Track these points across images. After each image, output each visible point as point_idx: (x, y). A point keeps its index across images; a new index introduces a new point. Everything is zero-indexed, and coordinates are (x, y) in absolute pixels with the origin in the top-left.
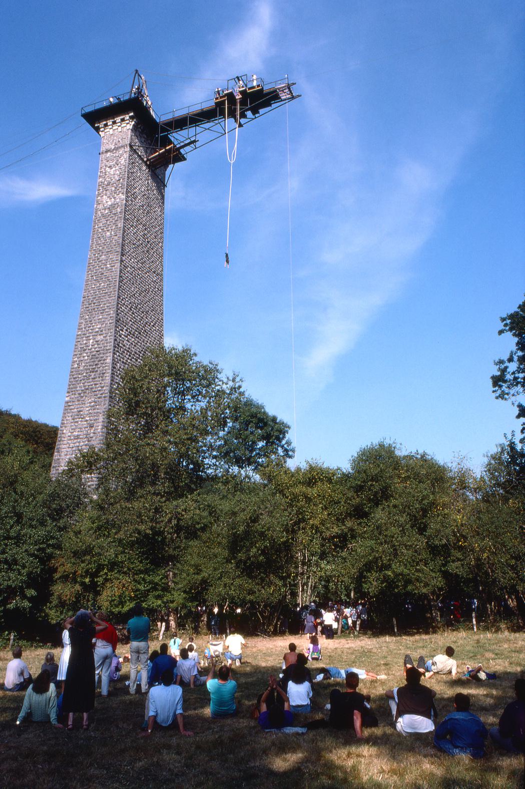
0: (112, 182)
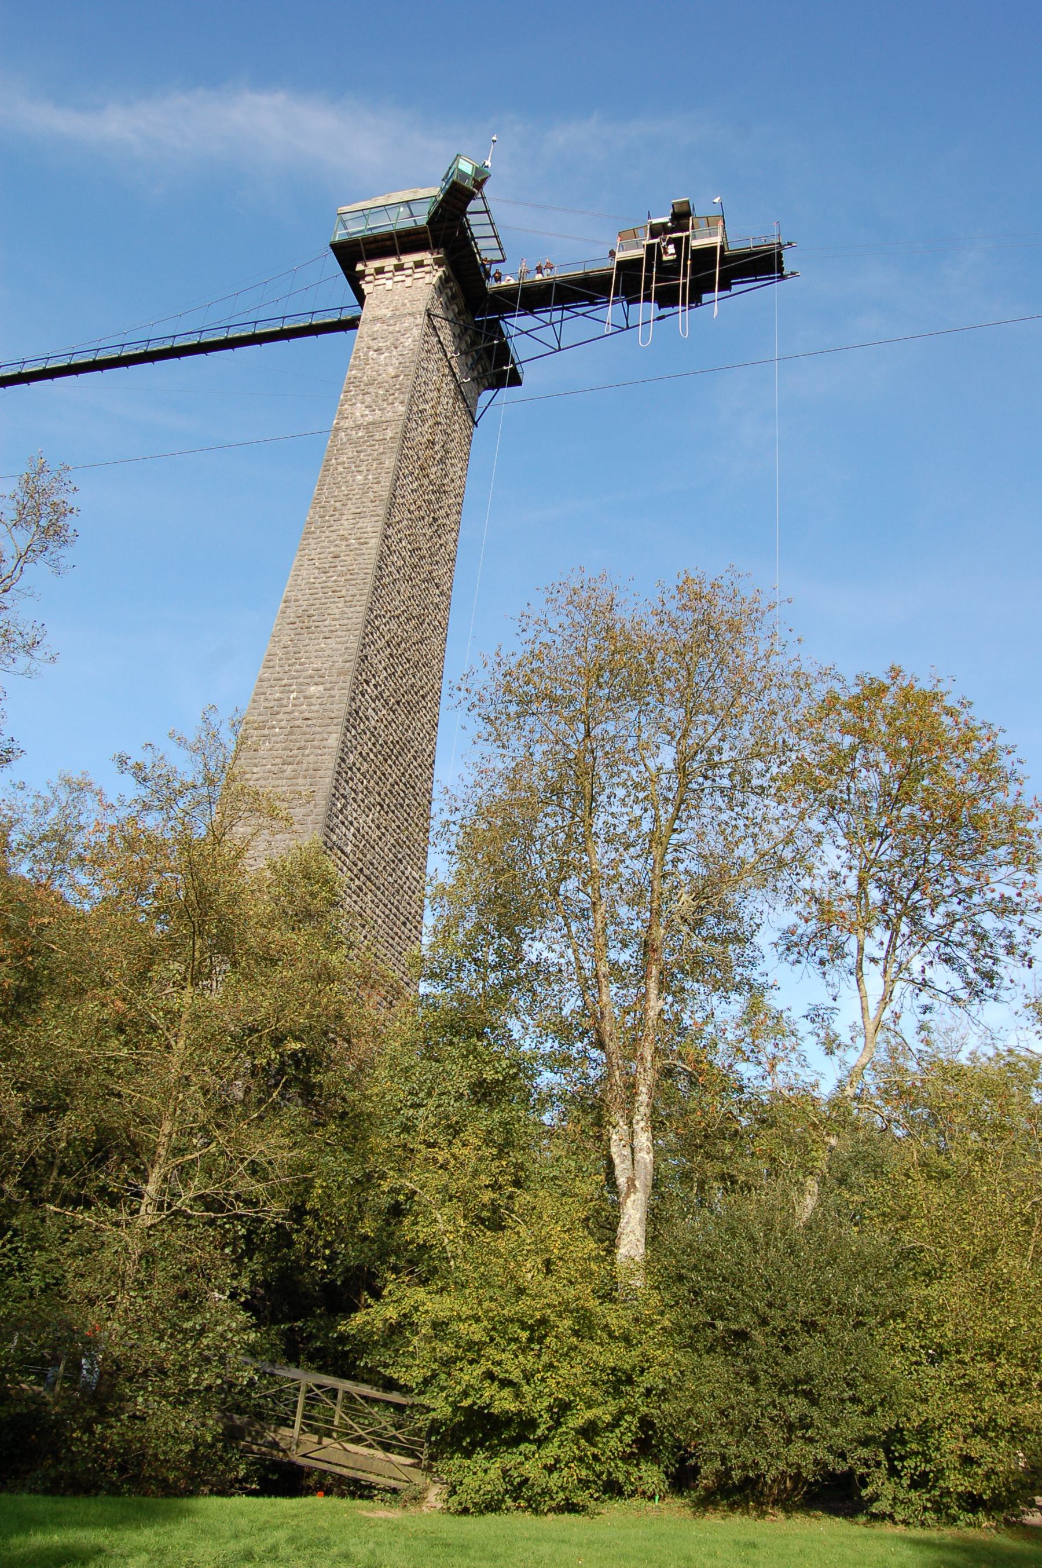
0: (380, 379)
